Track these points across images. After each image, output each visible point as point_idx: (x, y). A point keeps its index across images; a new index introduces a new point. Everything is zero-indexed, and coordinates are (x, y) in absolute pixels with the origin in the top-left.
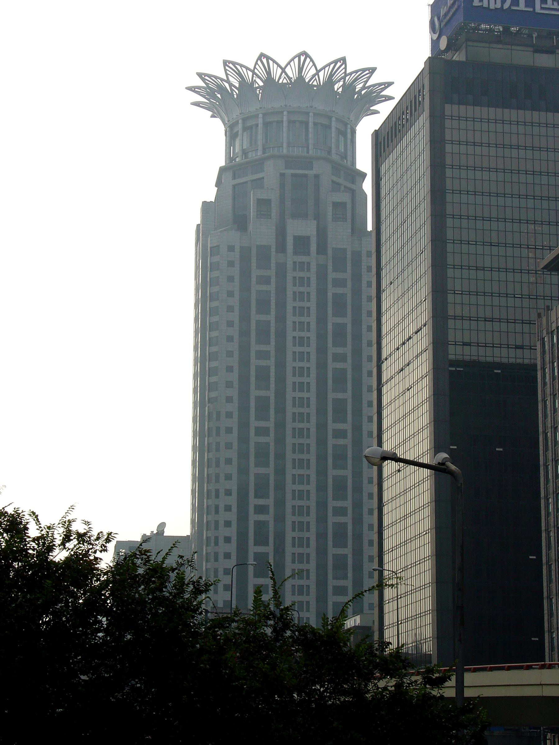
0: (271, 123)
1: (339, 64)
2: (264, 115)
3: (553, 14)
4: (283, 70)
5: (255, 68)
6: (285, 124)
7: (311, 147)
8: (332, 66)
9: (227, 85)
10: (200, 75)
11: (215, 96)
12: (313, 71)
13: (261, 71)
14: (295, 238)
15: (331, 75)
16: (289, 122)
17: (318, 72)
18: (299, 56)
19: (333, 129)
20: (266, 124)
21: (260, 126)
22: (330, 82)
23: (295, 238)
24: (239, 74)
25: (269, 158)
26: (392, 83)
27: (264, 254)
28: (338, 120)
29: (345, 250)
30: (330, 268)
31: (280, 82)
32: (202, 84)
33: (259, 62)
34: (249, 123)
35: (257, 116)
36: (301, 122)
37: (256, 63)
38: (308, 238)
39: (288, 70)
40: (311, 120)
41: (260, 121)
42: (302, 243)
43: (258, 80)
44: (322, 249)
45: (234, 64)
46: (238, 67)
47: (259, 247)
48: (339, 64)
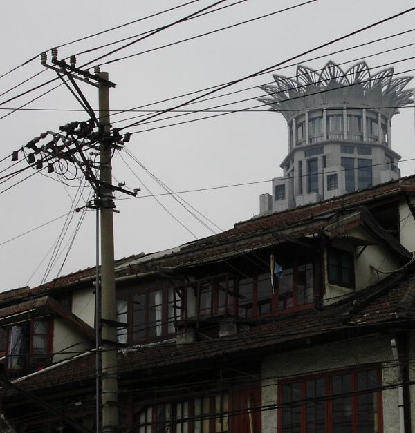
0: (315, 118)
13: (326, 75)
21: (307, 122)
25: (326, 143)
41: (307, 117)
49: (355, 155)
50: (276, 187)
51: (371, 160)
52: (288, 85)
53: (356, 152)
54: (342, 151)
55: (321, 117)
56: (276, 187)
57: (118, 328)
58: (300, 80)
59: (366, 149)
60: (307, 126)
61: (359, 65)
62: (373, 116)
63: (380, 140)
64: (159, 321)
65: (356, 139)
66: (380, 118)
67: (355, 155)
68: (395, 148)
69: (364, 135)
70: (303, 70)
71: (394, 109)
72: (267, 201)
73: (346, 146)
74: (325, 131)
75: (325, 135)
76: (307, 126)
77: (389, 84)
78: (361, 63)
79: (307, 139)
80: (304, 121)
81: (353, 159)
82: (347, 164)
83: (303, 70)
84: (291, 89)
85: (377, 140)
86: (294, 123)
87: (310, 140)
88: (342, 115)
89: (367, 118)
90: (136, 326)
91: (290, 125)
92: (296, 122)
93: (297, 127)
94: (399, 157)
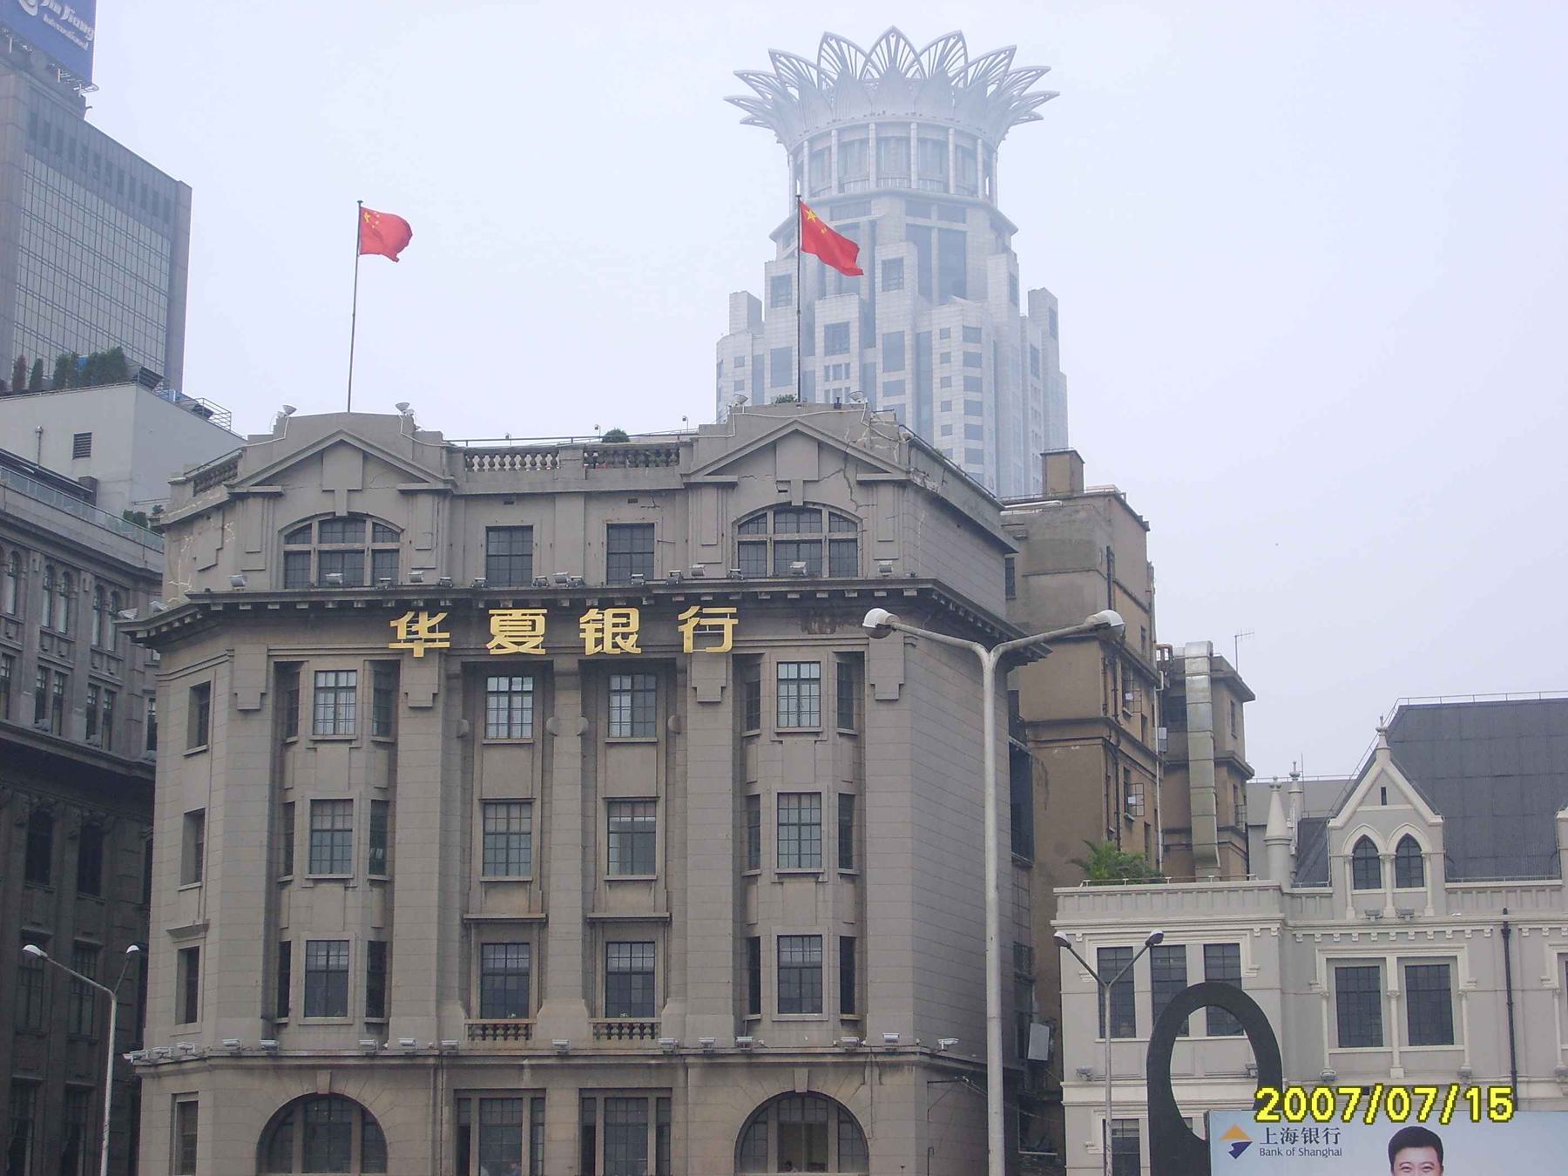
0: (852, 143)
1: (952, 41)
2: (840, 132)
3: (983, 1029)
4: (917, 58)
5: (873, 49)
6: (872, 143)
7: (914, 177)
8: (941, 45)
9: (814, 73)
10: (774, 56)
11: (784, 100)
12: (861, 60)
13: (881, 59)
14: (827, 327)
15: (987, 72)
16: (879, 140)
17: (968, 65)
18: (886, 36)
19: (951, 147)
20: (844, 146)
21: (834, 149)
22: (983, 79)
23: (827, 327)
24: (842, 59)
25: (878, 195)
26: (1057, 95)
27: (780, 357)
28: (958, 133)
29: (902, 334)
30: (880, 367)
31: (909, 75)
32: (771, 70)
33: (883, 42)
34: (818, 147)
35: (829, 134)
36: (899, 139)
37: (878, 43)
38: (846, 325)
39: (924, 59)
40: (913, 134)
41: (834, 141)
42: (837, 334)
43: (873, 71)
44: (868, 340)
45: (787, 57)
46: (844, 46)
47: (774, 353)
48: (952, 41)
49: (933, 221)
50: (773, 279)
51: (964, 233)
52: (798, 74)
53: (934, 216)
54: (909, 213)
55: (864, 142)
56: (773, 279)
57: (447, 645)
58: (824, 64)
59: (955, 210)
60: (835, 158)
61: (947, 39)
62: (967, 145)
63: (980, 193)
64: (621, 692)
65: (931, 189)
66: (980, 149)
67: (933, 221)
68: (1005, 206)
69: (952, 183)
70: (833, 43)
71: (980, 156)
72: (744, 312)
73: (917, 205)
74: (873, 170)
75: (873, 178)
76: (835, 158)
77: (1001, 81)
78: (953, 36)
79: (835, 183)
80: (830, 148)
81: (929, 229)
82: (916, 235)
83: (833, 43)
84: (803, 82)
85: (974, 192)
86: (806, 151)
87: (841, 187)
88: (908, 140)
89: (957, 147)
90: (745, 666)
91: (795, 153)
92: (811, 147)
93: (814, 156)
94: (1014, 230)
